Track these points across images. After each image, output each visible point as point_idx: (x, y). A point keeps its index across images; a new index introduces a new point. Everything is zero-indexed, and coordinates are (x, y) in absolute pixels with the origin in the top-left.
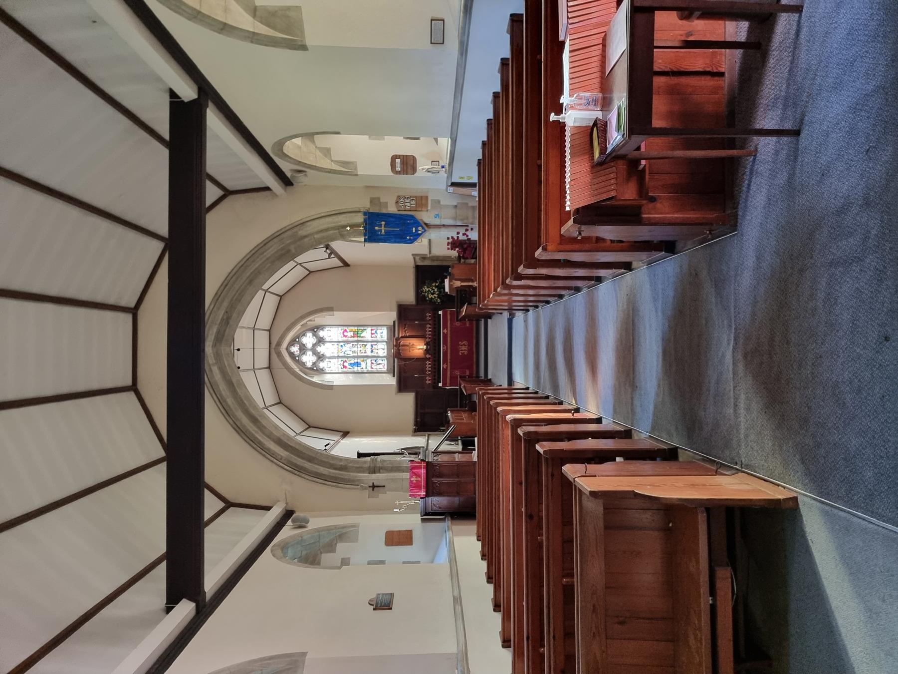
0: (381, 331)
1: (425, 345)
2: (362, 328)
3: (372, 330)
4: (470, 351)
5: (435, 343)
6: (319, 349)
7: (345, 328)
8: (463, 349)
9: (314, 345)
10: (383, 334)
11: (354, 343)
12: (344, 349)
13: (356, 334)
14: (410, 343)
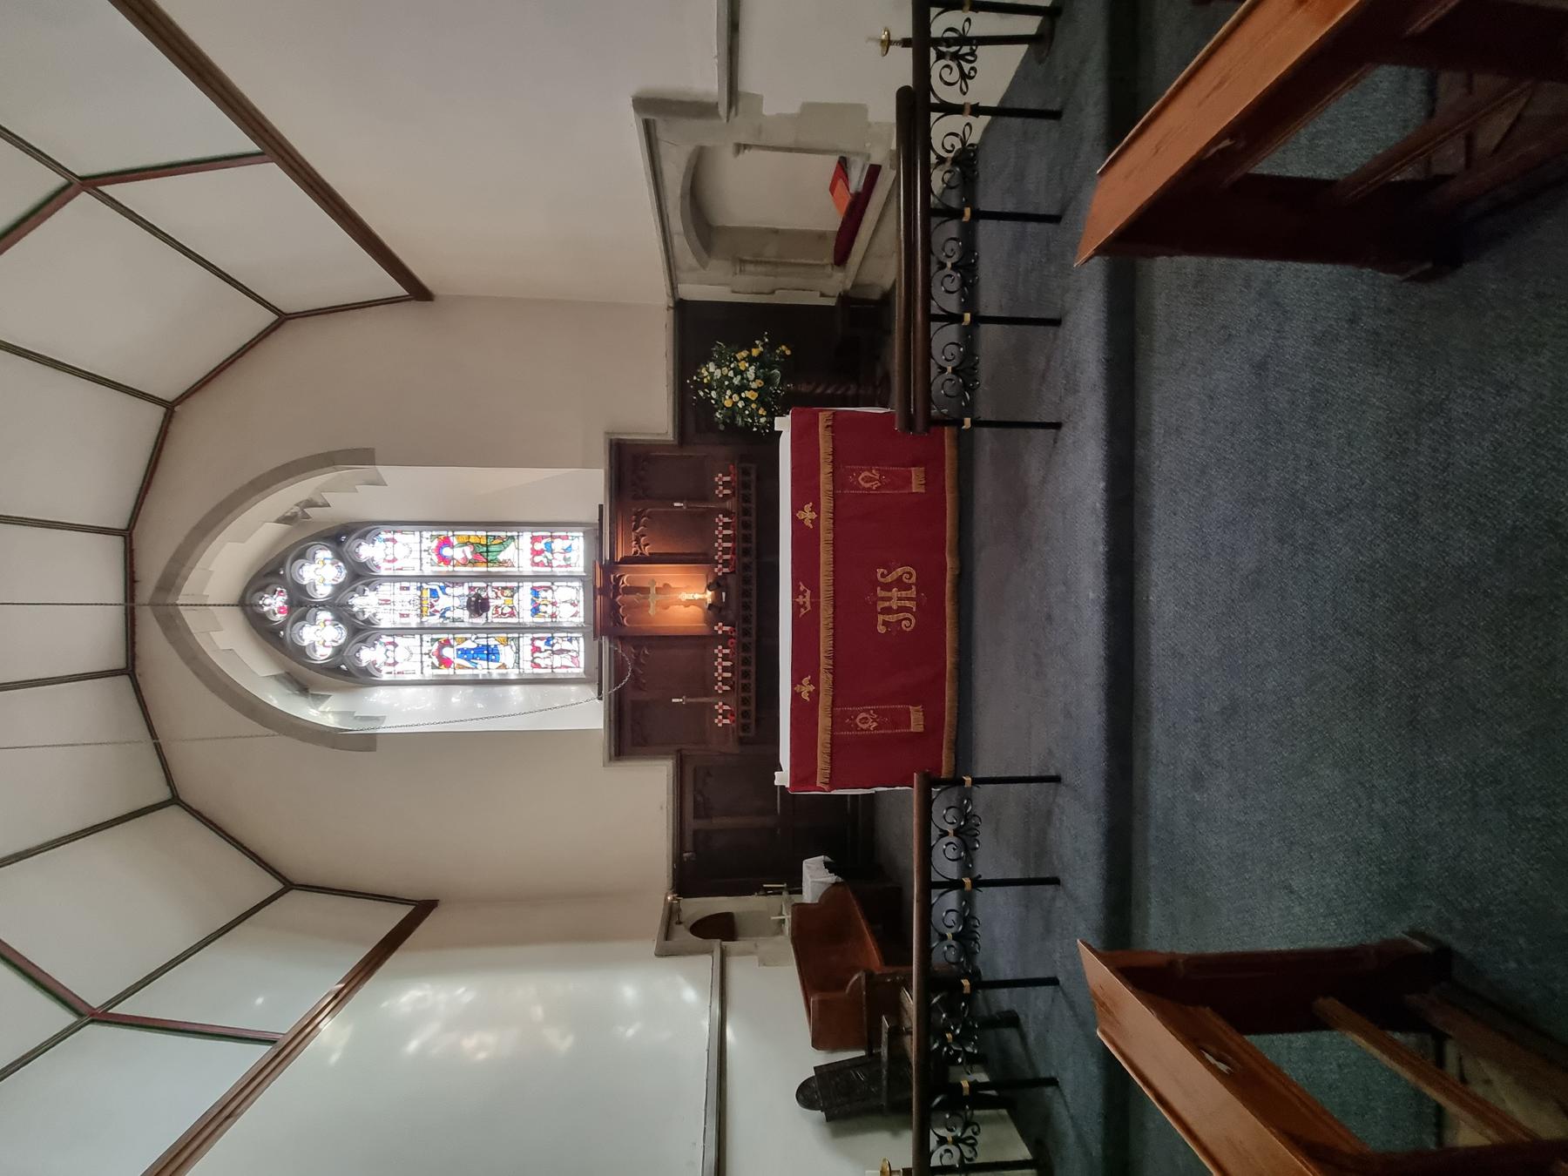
0: (566, 544)
1: (709, 587)
2: (503, 534)
3: (535, 540)
4: (929, 610)
5: (746, 581)
6: (357, 602)
7: (444, 533)
8: (894, 605)
9: (339, 588)
10: (573, 552)
11: (475, 584)
12: (443, 602)
13: (483, 554)
14: (654, 582)
